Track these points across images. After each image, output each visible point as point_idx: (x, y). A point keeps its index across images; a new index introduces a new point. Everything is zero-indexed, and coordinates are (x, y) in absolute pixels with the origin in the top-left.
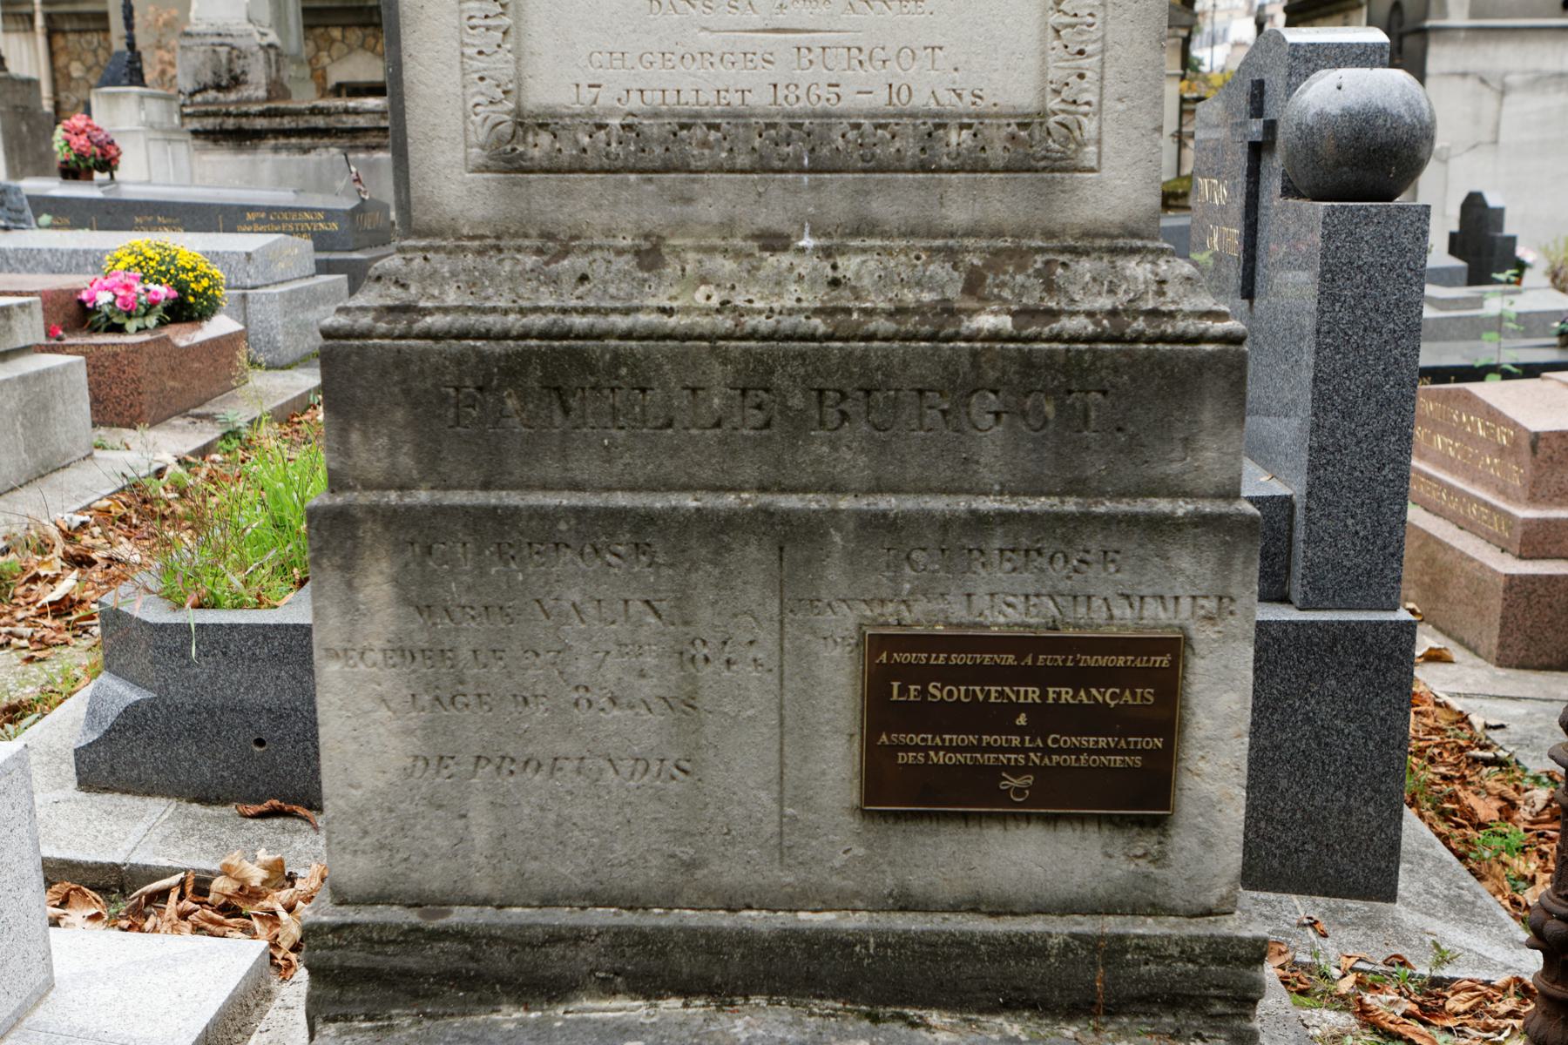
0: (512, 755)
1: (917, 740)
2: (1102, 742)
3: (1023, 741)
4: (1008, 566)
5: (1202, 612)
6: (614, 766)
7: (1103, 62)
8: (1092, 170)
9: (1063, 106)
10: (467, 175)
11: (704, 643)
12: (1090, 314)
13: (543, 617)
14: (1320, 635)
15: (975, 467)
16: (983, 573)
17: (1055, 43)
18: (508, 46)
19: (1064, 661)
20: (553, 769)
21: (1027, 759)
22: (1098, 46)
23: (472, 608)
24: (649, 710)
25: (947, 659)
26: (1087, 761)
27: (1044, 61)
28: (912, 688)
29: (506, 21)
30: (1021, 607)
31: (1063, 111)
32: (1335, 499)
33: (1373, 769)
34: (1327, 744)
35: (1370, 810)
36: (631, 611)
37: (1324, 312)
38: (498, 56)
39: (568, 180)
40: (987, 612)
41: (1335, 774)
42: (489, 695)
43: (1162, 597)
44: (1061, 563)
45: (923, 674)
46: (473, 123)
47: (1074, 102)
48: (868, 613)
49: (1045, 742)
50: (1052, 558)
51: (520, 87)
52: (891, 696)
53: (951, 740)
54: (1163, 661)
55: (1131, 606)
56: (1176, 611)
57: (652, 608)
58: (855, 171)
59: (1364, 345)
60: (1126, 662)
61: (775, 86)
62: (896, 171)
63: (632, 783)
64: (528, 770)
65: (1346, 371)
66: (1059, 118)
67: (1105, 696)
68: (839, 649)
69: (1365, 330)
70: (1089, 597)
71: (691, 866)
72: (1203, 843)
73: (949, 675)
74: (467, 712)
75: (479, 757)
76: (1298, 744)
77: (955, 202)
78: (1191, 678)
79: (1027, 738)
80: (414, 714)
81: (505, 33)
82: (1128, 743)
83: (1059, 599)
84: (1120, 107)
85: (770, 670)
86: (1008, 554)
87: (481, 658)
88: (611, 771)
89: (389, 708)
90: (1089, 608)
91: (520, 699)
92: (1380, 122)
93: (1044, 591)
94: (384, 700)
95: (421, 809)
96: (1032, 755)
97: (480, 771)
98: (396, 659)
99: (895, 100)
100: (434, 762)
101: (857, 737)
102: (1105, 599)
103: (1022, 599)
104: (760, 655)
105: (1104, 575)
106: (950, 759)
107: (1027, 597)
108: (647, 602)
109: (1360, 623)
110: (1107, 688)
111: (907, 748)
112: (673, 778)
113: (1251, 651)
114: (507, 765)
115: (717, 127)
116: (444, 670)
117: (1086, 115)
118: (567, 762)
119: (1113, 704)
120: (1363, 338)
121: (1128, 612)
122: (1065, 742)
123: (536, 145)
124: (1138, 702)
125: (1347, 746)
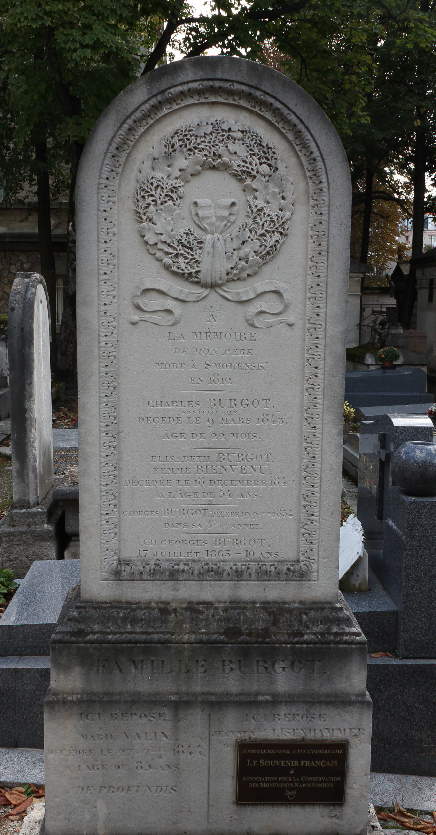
0: (114, 786)
1: (256, 779)
2: (320, 779)
3: (292, 779)
4: (287, 719)
5: (353, 734)
6: (150, 789)
7: (319, 546)
8: (315, 581)
9: (305, 559)
10: (101, 582)
11: (182, 746)
12: (314, 634)
13: (126, 738)
14: (408, 670)
15: (276, 685)
16: (279, 722)
17: (303, 539)
18: (116, 538)
19: (307, 752)
20: (128, 790)
21: (294, 785)
22: (317, 541)
23: (101, 735)
24: (163, 769)
25: (267, 751)
26: (315, 785)
27: (299, 544)
28: (254, 761)
29: (116, 530)
30: (292, 733)
31: (305, 560)
32: (414, 614)
33: (430, 723)
34: (412, 713)
35: (430, 740)
36: (157, 736)
37: (408, 542)
38: (113, 542)
39: (136, 583)
40: (280, 735)
41: (416, 725)
42: (106, 765)
43: (340, 729)
44: (305, 718)
45: (258, 757)
46: (103, 564)
47: (309, 558)
48: (239, 736)
49: (300, 779)
50: (302, 716)
51: (119, 551)
52: (247, 764)
53: (268, 779)
54: (340, 751)
55: (329, 732)
56: (344, 733)
57: (165, 735)
58: (235, 581)
59: (424, 555)
60: (328, 752)
61: (208, 551)
62: (249, 581)
63: (156, 795)
64: (119, 791)
65: (417, 565)
66: (304, 562)
67: (321, 763)
68: (229, 748)
69: (424, 549)
70: (315, 729)
71: (175, 823)
72: (355, 812)
73: (267, 757)
74: (98, 771)
75: (102, 787)
76: (400, 713)
77: (269, 591)
78: (350, 756)
79: (294, 778)
80: (79, 772)
81: (115, 534)
82: (328, 779)
83: (305, 730)
84: (324, 561)
85: (205, 755)
86: (288, 715)
87: (104, 752)
88: (149, 791)
89: (70, 770)
90: (315, 733)
91: (117, 766)
92: (431, 469)
93: (300, 728)
94: (69, 767)
95: (80, 805)
96: (296, 784)
97: (102, 791)
98: (74, 753)
99: (248, 556)
100: (85, 789)
101: (235, 778)
102: (320, 730)
103: (292, 730)
104: (202, 750)
105: (320, 722)
106: (267, 785)
107: (294, 730)
108: (163, 733)
109: (424, 665)
110: (321, 761)
111: (252, 782)
112: (170, 793)
113: (370, 746)
114: (112, 789)
115: (188, 565)
116: (90, 757)
117: (313, 563)
118: (133, 788)
119: (323, 766)
120: (423, 552)
121: (328, 734)
122: (307, 779)
123: (125, 571)
124: (332, 765)
125: (420, 714)
